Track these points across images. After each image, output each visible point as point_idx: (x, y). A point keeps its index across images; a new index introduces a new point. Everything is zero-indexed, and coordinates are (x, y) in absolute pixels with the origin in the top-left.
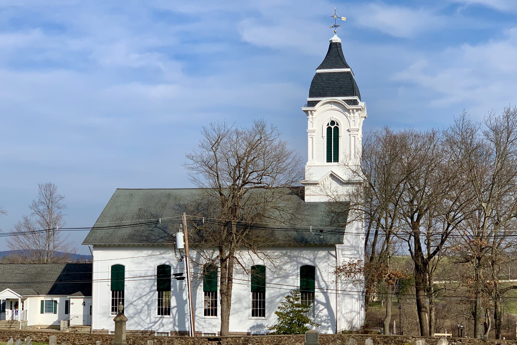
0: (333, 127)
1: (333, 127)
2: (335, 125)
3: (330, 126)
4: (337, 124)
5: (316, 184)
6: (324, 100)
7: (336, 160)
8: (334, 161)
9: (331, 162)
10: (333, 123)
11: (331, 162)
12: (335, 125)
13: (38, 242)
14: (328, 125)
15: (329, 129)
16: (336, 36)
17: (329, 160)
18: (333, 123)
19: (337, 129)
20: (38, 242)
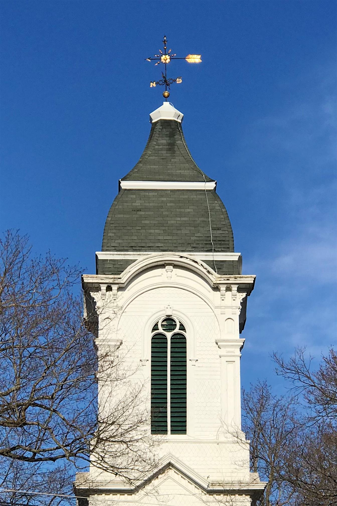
0: (169, 335)
1: (169, 335)
2: (177, 330)
3: (161, 330)
4: (182, 328)
5: (105, 319)
6: (143, 259)
7: (180, 427)
8: (174, 431)
9: (165, 432)
10: (169, 322)
11: (165, 432)
12: (177, 330)
13: (3, 329)
14: (155, 328)
15: (158, 342)
16: (166, 105)
17: (158, 427)
18: (169, 322)
19: (180, 342)
20: (3, 329)
